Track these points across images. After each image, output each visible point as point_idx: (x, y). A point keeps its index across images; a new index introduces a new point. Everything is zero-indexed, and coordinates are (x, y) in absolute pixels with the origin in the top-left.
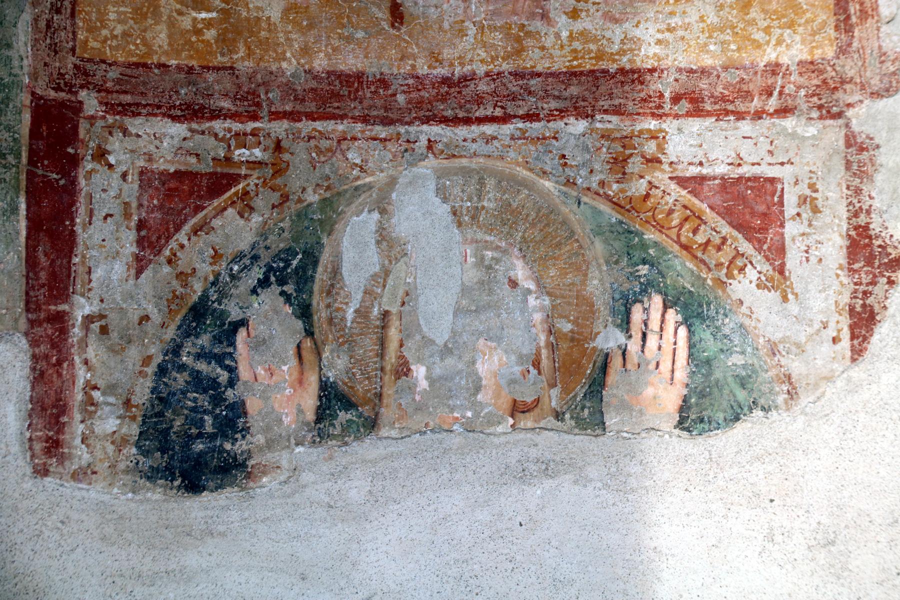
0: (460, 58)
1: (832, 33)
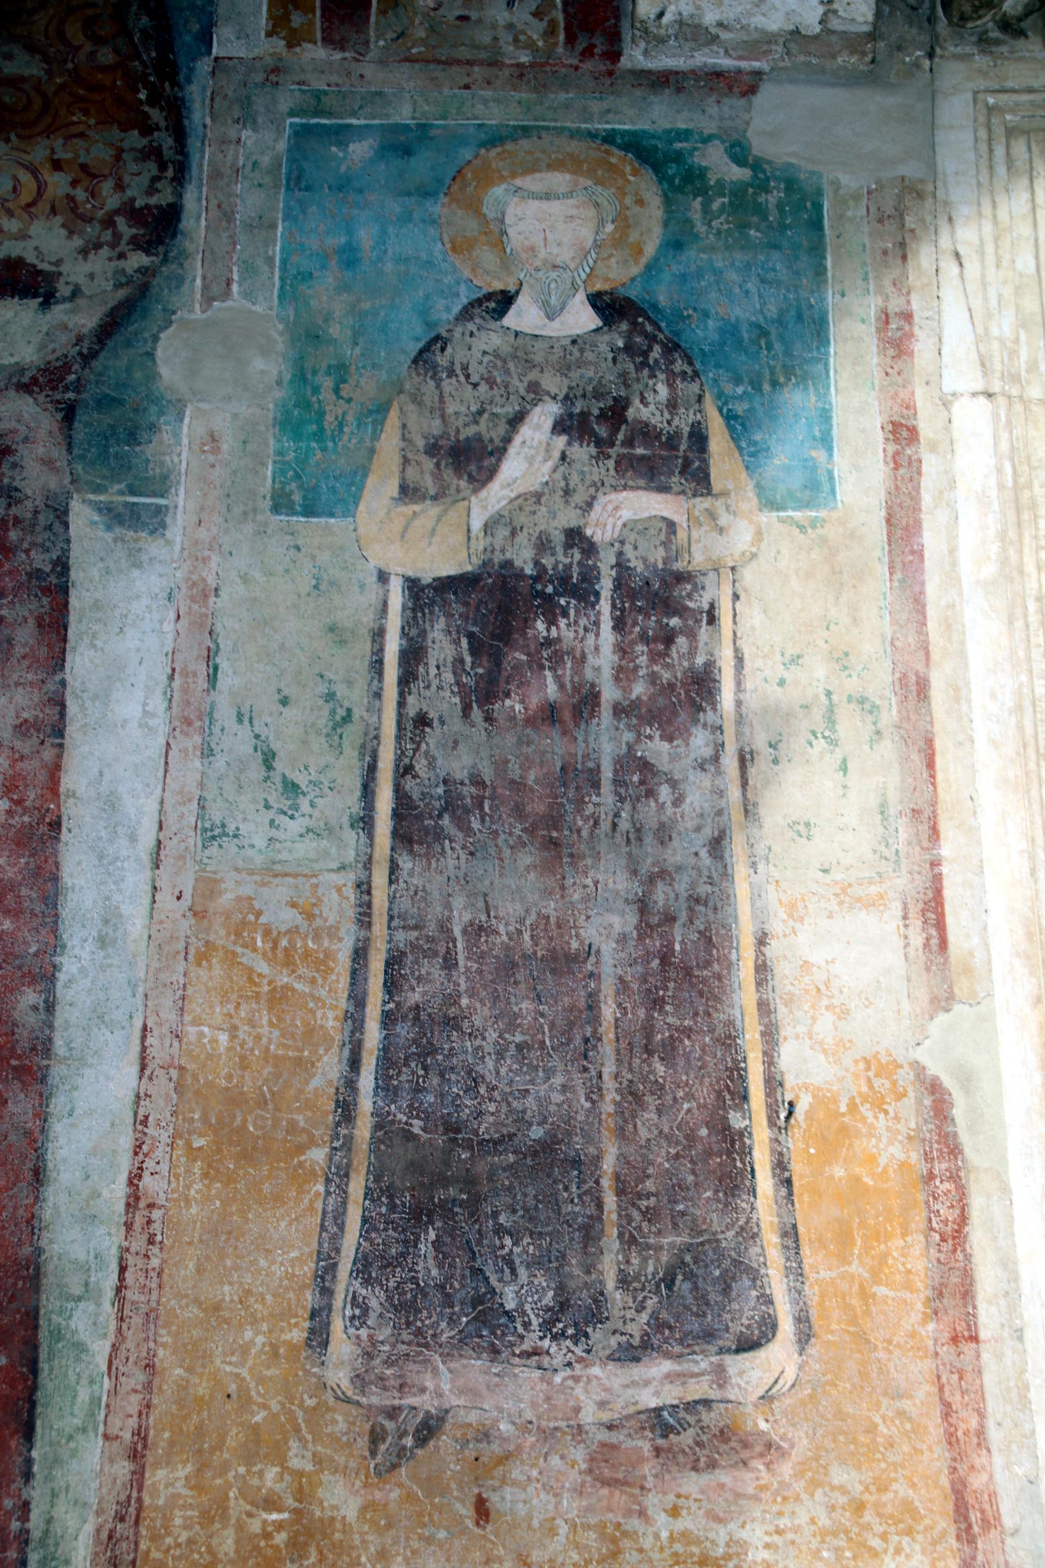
0: (550, 1561)
1: (953, 1542)
